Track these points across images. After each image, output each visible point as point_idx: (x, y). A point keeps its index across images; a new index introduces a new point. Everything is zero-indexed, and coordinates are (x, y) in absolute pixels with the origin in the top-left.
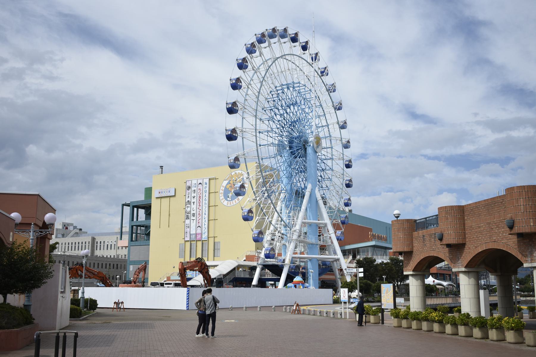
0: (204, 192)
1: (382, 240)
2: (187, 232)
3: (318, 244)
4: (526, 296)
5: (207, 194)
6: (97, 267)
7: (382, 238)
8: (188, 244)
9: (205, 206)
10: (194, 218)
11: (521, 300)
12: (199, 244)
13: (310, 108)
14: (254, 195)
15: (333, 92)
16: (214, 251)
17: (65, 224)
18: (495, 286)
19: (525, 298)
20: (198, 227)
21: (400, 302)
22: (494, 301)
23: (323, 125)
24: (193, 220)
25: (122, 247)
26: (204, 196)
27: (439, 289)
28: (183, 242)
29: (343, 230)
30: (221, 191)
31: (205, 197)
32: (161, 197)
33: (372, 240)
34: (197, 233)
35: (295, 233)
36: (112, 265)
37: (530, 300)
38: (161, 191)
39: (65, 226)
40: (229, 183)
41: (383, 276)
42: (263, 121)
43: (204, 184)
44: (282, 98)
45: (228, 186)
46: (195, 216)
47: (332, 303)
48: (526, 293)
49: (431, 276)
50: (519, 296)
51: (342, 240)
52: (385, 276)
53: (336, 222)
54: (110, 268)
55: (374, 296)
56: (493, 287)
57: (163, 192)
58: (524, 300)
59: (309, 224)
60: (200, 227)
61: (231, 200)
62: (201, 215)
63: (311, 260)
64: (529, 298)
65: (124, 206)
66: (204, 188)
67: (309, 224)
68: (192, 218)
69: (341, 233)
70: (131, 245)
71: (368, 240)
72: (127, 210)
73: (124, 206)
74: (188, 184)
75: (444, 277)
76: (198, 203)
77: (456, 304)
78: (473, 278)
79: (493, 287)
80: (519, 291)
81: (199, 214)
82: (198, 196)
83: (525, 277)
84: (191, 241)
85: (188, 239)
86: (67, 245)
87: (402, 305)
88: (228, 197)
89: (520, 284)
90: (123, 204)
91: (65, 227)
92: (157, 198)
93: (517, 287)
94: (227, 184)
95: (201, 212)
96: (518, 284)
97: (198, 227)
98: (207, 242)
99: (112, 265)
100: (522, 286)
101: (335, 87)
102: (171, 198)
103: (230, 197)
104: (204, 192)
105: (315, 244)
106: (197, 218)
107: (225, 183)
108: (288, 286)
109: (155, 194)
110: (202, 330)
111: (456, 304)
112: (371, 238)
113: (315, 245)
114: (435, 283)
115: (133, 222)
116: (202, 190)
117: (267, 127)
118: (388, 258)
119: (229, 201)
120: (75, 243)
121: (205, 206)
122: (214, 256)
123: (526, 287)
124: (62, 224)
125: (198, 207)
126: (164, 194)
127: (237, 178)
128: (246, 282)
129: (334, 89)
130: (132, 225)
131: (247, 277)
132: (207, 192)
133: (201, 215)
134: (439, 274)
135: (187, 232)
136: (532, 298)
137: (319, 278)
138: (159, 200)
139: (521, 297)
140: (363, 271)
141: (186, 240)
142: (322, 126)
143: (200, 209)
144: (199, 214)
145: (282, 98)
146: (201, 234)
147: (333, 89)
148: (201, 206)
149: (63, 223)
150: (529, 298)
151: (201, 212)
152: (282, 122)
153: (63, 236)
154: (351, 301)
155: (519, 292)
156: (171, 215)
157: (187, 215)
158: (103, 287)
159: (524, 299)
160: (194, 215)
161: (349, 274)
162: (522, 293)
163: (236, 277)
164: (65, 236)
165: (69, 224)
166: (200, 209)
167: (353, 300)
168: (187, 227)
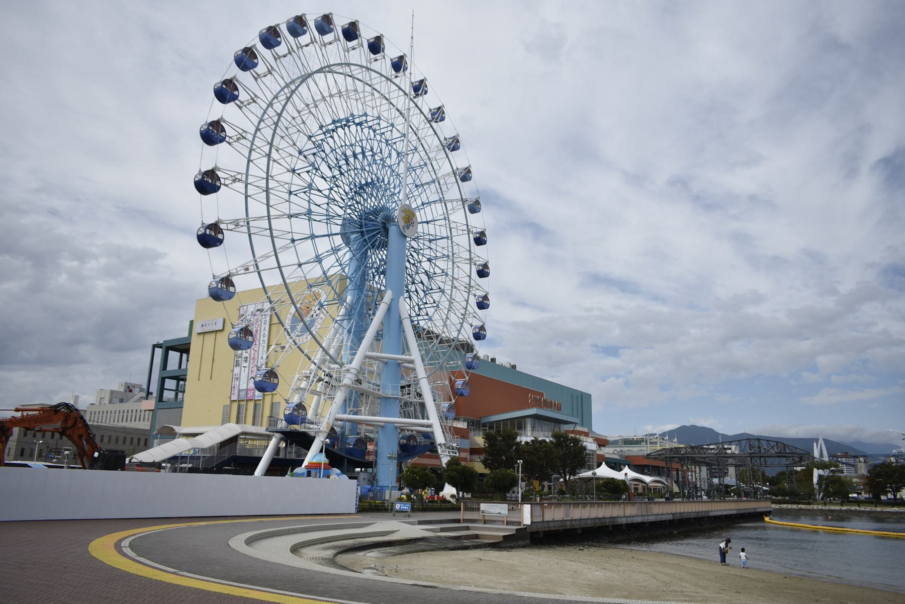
0: (263, 324)
1: (551, 408)
2: (234, 387)
3: (398, 398)
4: (779, 502)
5: (267, 327)
6: (143, 445)
7: (551, 405)
8: (235, 405)
9: (263, 345)
10: (246, 365)
11: (774, 509)
12: (251, 405)
13: (389, 142)
14: (264, 294)
15: (440, 121)
17: (129, 385)
18: (734, 486)
19: (779, 506)
20: (251, 378)
21: (500, 513)
22: (731, 510)
23: (423, 183)
24: (245, 367)
25: (145, 410)
26: (262, 329)
27: (651, 488)
28: (228, 403)
29: (467, 378)
31: (264, 332)
32: (204, 333)
33: (533, 407)
35: (348, 375)
37: (786, 509)
38: (204, 323)
39: (128, 387)
41: (518, 461)
42: (443, 272)
44: (356, 139)
46: (248, 362)
47: (353, 511)
48: (780, 498)
49: (626, 466)
50: (770, 502)
51: (465, 394)
52: (521, 461)
53: (454, 364)
55: (506, 498)
56: (732, 488)
57: (207, 325)
58: (778, 509)
59: (383, 362)
62: (256, 359)
63: (383, 427)
64: (784, 506)
65: (156, 348)
67: (383, 362)
68: (244, 364)
69: (464, 382)
70: (159, 407)
71: (528, 407)
72: (159, 352)
73: (156, 348)
74: (242, 312)
75: (659, 471)
77: (646, 518)
78: (351, 296)
79: (732, 488)
80: (770, 495)
83: (776, 476)
84: (239, 401)
85: (235, 397)
86: (121, 414)
87: (504, 521)
89: (770, 484)
90: (154, 345)
91: (128, 389)
92: (199, 334)
93: (765, 488)
95: (256, 354)
96: (768, 484)
98: (262, 402)
100: (774, 488)
101: (443, 113)
102: (219, 334)
104: (263, 324)
105: (390, 398)
108: (297, 473)
109: (197, 329)
111: (646, 518)
112: (531, 403)
113: (392, 399)
114: (628, 478)
115: (165, 371)
118: (550, 434)
120: (132, 410)
121: (263, 345)
123: (779, 489)
124: (124, 385)
126: (205, 328)
128: (247, 465)
129: (442, 116)
130: (163, 376)
131: (293, 458)
132: (268, 323)
133: (256, 359)
134: (652, 466)
135: (234, 387)
136: (790, 505)
138: (201, 337)
139: (773, 503)
140: (165, 391)
141: (232, 399)
142: (422, 184)
143: (255, 349)
145: (356, 140)
147: (440, 118)
148: (257, 346)
149: (126, 383)
150: (785, 505)
151: (256, 354)
153: (121, 401)
154: (397, 508)
155: (768, 496)
156: (215, 360)
157: (237, 360)
158: (79, 468)
159: (777, 506)
160: (247, 360)
161: (447, 455)
162: (774, 498)
163: (237, 454)
164: (125, 401)
165: (134, 386)
166: (256, 351)
167: (400, 506)
168: (235, 378)
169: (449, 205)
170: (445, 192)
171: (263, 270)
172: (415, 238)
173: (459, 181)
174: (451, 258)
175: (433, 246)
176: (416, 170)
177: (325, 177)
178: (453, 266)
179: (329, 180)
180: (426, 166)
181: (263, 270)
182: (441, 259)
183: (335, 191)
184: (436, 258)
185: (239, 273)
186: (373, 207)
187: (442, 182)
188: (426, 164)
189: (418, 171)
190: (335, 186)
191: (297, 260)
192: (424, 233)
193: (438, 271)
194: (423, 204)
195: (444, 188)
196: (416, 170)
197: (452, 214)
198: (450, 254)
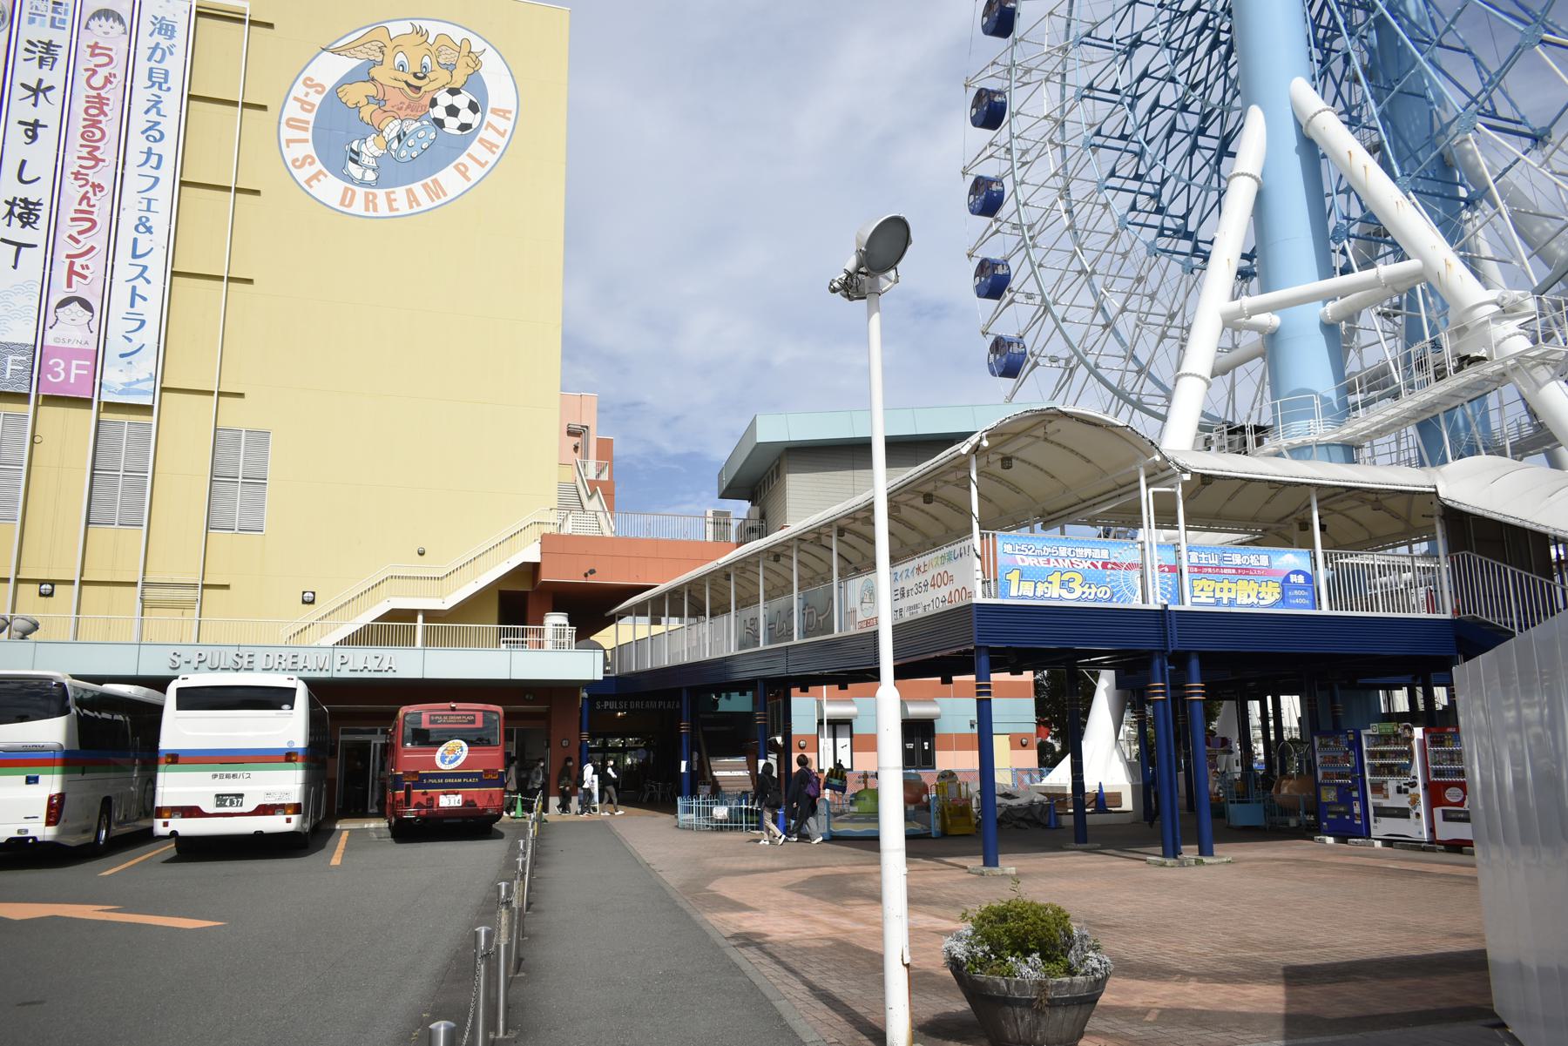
16: (92, 475)
20: (64, 303)
30: (292, 110)
34: (49, 341)
36: (567, 646)
40: (363, 74)
43: (146, 27)
45: (357, 93)
46: (42, 223)
54: (989, 686)
60: (86, 305)
61: (378, 183)
66: (143, 53)
76: (76, 140)
81: (85, 216)
82: (82, 92)
88: (355, 162)
94: (349, 79)
97: (64, 303)
99: (567, 646)
103: (365, 159)
106: (62, 237)
107: (330, 70)
110: (1414, 957)
116: (119, 59)
117: (1167, 105)
119: (362, 183)
122: (88, 523)
125: (73, 165)
127: (426, 60)
137: (684, 692)
144: (85, 216)
146: (97, 358)
152: (1222, 113)
166: (97, 187)
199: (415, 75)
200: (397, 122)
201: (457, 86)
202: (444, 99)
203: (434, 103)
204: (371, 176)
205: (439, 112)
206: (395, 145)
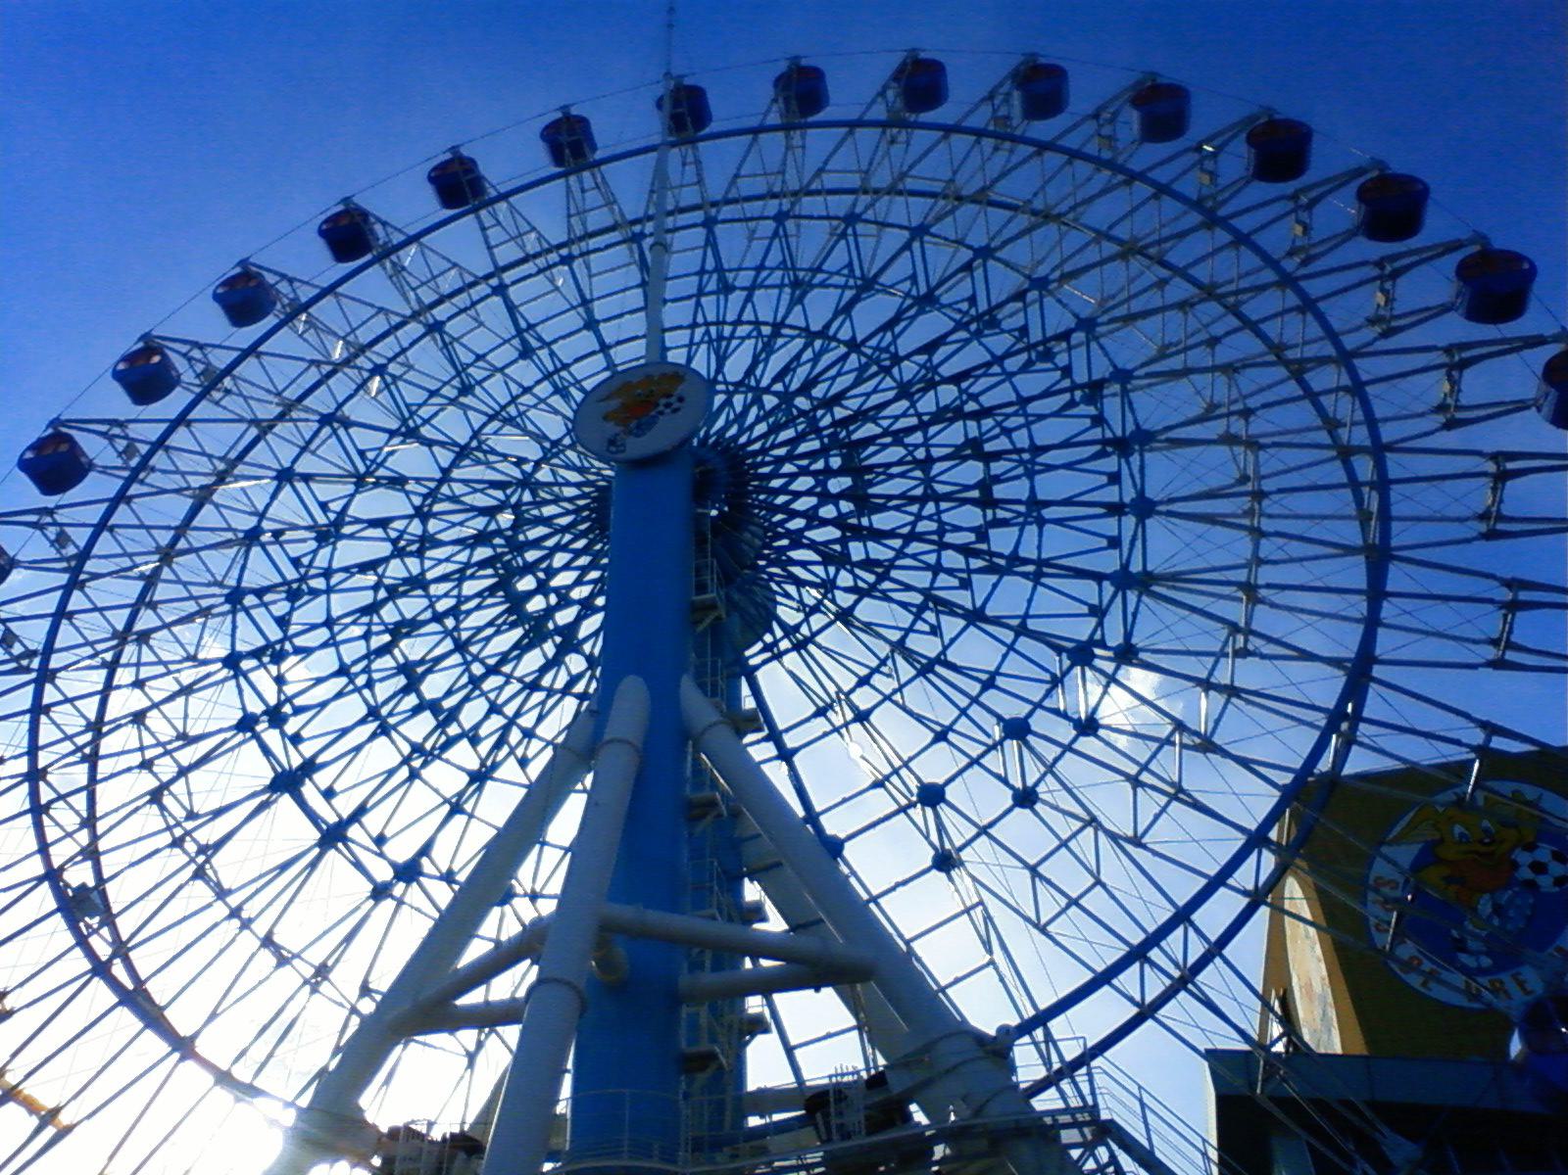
61: (1499, 967)
94: (1418, 865)
169: (507, 253)
170: (466, 275)
171: (957, 981)
172: (717, 353)
173: (1043, 129)
174: (786, 204)
175: (745, 278)
176: (407, 406)
177: (897, 329)
178: (818, 192)
179: (884, 344)
180: (384, 366)
181: (957, 981)
182: (793, 241)
183: (540, 718)
184: (787, 265)
185: (1032, 624)
186: (597, 556)
187: (428, 297)
188: (378, 370)
189: (413, 396)
190: (864, 360)
191: (894, 820)
192: (694, 325)
193: (838, 258)
194: (526, 353)
195: (449, 282)
196: (407, 406)
197: (540, 237)
198: (772, 207)
199: (1481, 842)
200: (1487, 896)
201: (1531, 839)
202: (1523, 858)
203: (1515, 866)
204: (1486, 962)
205: (1526, 873)
206: (1496, 922)
